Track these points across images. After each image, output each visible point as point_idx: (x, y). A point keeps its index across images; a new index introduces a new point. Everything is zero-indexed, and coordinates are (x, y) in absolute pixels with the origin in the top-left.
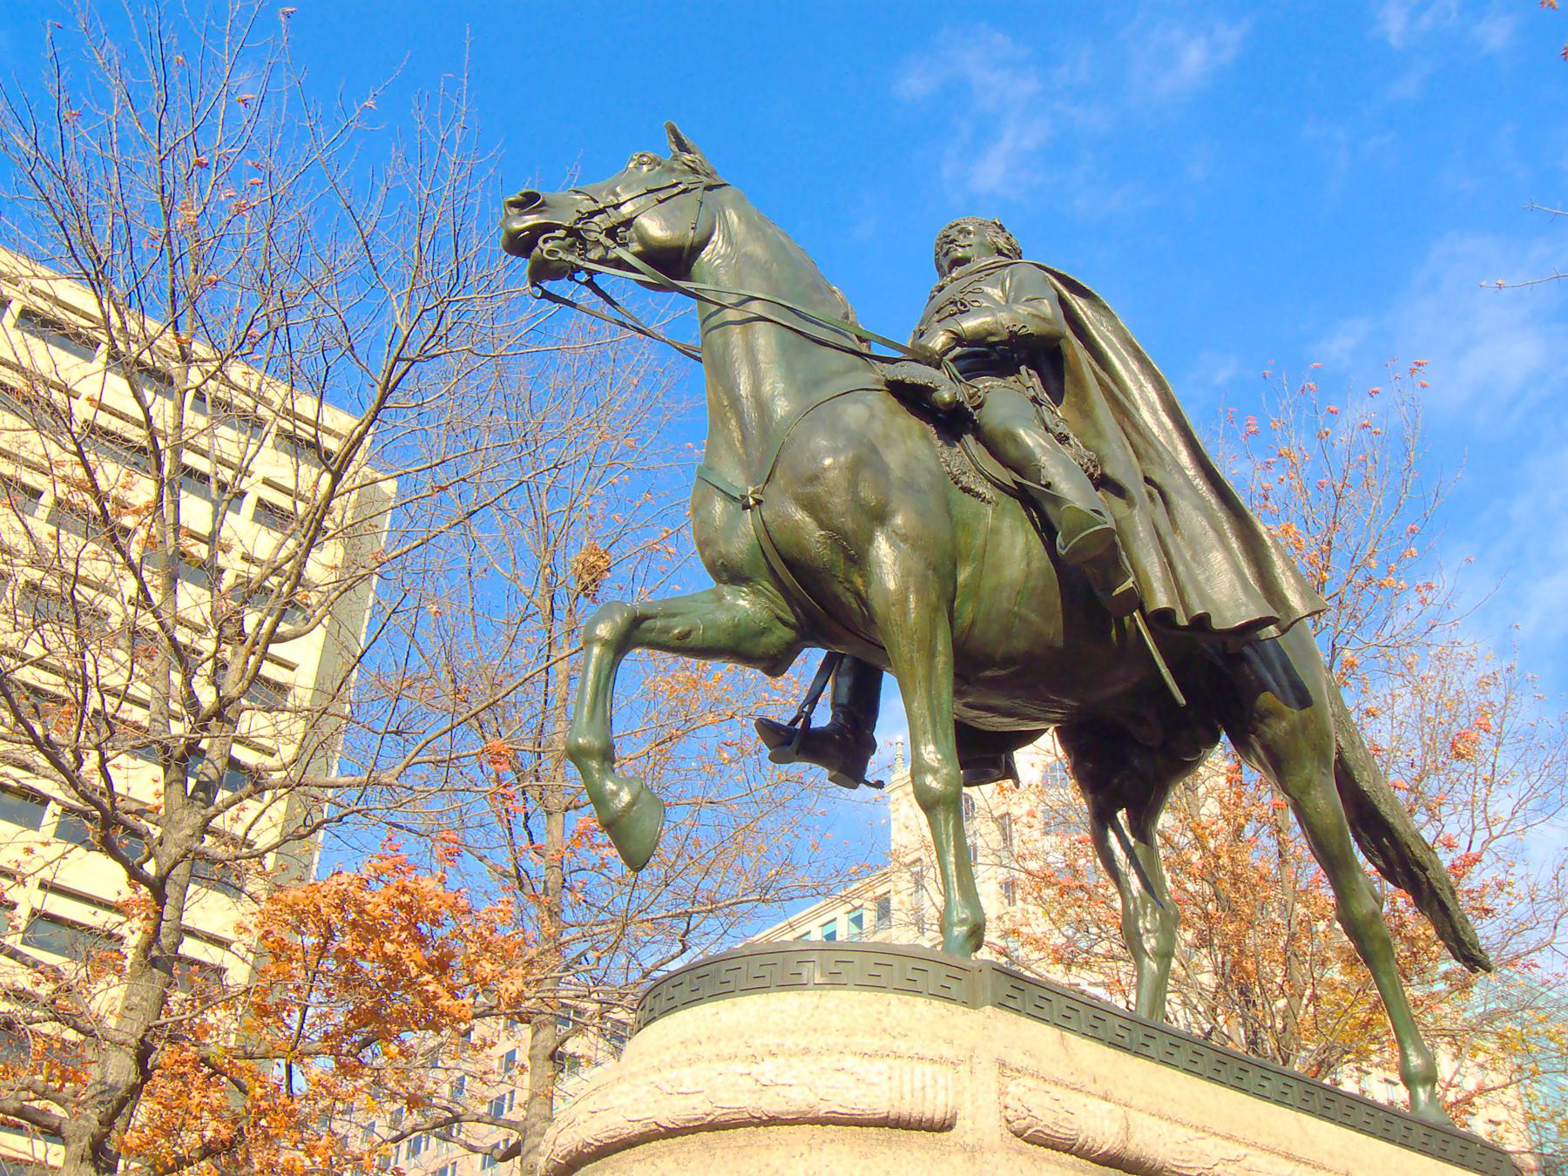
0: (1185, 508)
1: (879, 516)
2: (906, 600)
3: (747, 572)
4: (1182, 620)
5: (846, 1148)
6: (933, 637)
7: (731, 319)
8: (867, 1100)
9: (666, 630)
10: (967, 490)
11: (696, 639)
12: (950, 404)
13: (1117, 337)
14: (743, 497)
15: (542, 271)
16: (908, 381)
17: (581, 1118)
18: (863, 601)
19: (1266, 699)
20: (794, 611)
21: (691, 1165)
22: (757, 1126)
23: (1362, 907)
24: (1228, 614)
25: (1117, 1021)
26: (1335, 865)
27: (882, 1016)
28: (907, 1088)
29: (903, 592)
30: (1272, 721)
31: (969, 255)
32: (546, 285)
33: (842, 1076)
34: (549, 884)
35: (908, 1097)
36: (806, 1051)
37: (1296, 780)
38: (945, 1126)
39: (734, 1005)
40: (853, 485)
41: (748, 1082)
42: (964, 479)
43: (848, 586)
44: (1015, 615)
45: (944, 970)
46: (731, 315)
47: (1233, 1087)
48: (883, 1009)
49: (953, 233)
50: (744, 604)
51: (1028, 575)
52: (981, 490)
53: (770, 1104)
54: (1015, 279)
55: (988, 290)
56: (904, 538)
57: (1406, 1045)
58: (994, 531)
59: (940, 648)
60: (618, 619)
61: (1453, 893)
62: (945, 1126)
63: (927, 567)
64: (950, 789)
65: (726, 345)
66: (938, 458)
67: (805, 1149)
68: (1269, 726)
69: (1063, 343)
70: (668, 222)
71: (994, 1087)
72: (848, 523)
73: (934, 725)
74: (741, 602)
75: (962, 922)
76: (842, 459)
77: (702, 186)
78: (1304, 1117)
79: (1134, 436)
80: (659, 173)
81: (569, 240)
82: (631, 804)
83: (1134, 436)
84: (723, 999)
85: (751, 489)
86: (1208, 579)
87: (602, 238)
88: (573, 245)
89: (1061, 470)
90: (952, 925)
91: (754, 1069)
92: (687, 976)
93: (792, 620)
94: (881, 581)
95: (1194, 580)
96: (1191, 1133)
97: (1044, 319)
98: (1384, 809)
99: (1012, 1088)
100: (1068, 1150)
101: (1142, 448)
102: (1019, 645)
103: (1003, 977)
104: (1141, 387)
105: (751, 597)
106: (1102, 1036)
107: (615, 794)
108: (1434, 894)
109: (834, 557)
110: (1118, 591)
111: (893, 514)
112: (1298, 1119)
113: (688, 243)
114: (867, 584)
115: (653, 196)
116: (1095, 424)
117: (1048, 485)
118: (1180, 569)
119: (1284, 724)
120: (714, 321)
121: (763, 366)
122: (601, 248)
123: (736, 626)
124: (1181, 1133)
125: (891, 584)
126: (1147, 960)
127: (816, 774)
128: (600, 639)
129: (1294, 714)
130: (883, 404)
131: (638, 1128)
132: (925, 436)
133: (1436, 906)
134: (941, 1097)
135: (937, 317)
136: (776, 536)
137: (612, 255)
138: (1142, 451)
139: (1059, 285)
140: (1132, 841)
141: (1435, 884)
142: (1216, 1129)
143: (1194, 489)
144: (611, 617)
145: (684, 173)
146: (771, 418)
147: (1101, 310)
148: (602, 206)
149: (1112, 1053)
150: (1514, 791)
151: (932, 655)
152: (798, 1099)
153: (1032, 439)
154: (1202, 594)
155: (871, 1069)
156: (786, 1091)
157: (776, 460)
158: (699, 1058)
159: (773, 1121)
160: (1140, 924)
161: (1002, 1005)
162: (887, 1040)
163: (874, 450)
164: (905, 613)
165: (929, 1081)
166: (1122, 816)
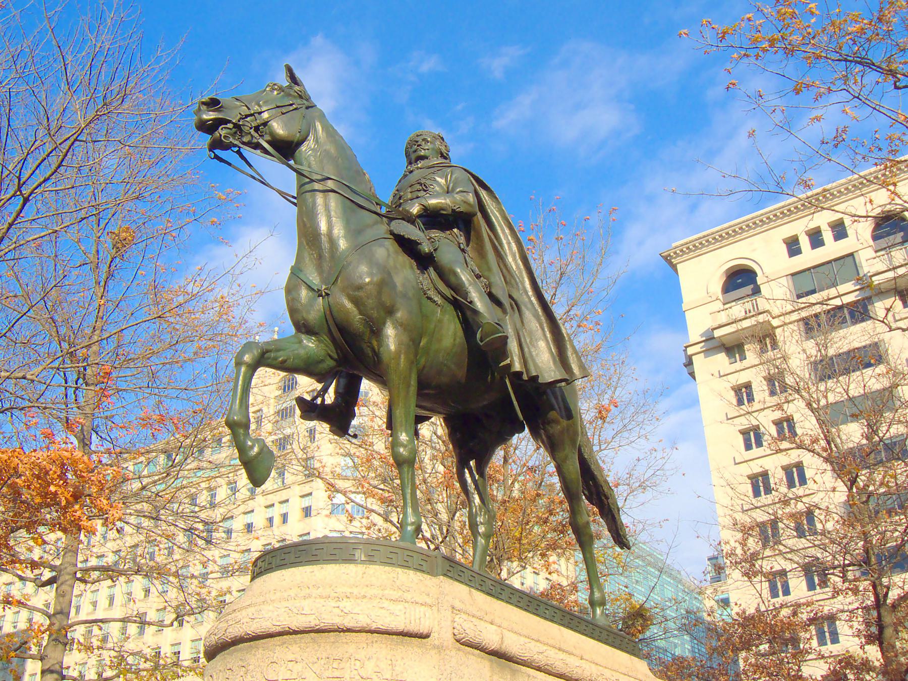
0: (528, 315)
1: (390, 311)
2: (400, 357)
3: (316, 330)
4: (525, 377)
5: (384, 646)
6: (410, 377)
7: (316, 188)
8: (394, 623)
9: (275, 359)
10: (429, 298)
11: (289, 364)
12: (426, 254)
13: (500, 214)
14: (319, 290)
15: (217, 145)
16: (406, 236)
17: (245, 620)
18: (376, 354)
19: (553, 414)
20: (337, 353)
21: (308, 650)
22: (340, 632)
23: (582, 520)
24: (546, 375)
25: (490, 582)
26: (571, 496)
27: (395, 580)
28: (413, 618)
29: (398, 353)
30: (554, 425)
31: (428, 155)
32: (218, 152)
33: (383, 611)
34: (85, 428)
35: (413, 622)
36: (365, 597)
37: (560, 455)
38: (427, 636)
39: (322, 568)
40: (380, 293)
41: (337, 611)
42: (428, 292)
43: (369, 344)
44: (445, 365)
45: (421, 557)
46: (317, 186)
47: (534, 614)
48: (395, 576)
49: (420, 139)
50: (310, 344)
51: (454, 345)
52: (436, 299)
53: (349, 623)
54: (454, 176)
55: (438, 179)
56: (401, 325)
57: (595, 590)
58: (440, 321)
59: (412, 383)
60: (256, 353)
61: (619, 511)
62: (427, 636)
63: (410, 340)
64: (412, 455)
65: (314, 203)
66: (417, 280)
67: (365, 645)
68: (552, 427)
69: (475, 219)
70: (285, 126)
71: (450, 618)
72: (375, 314)
73: (406, 421)
74: (310, 345)
75: (413, 524)
76: (375, 279)
77: (304, 107)
78: (562, 628)
79: (504, 271)
80: (283, 96)
81: (234, 130)
82: (259, 454)
83: (504, 271)
84: (316, 565)
85: (324, 287)
86: (537, 355)
87: (252, 131)
88: (236, 133)
89: (478, 295)
90: (407, 524)
91: (338, 604)
92: (293, 549)
93: (336, 356)
94: (388, 345)
95: (532, 356)
96: (527, 640)
97: (469, 204)
98: (593, 467)
99: (457, 619)
100: (476, 648)
101: (508, 277)
102: (444, 380)
103: (446, 561)
104: (509, 243)
105: (317, 343)
106: (484, 589)
107: (252, 447)
108: (610, 510)
109: (365, 330)
110: (502, 364)
111: (398, 310)
112: (559, 629)
113: (296, 140)
114: (380, 346)
115: (279, 110)
116: (487, 263)
117: (471, 302)
118: (526, 350)
119: (559, 427)
120: (308, 187)
121: (334, 219)
122: (249, 136)
123: (309, 358)
124: (523, 639)
125: (392, 347)
126: (479, 538)
127: (323, 428)
128: (246, 363)
129: (564, 422)
130: (391, 245)
131: (279, 629)
132: (412, 268)
133: (610, 517)
134: (427, 623)
135: (409, 190)
136: (335, 314)
137: (255, 141)
138: (508, 280)
139: (474, 182)
140: (477, 477)
141: (611, 506)
142: (533, 637)
143: (531, 302)
144: (252, 352)
145: (295, 97)
146: (337, 249)
147: (494, 200)
148: (252, 112)
149: (489, 598)
150: (615, 426)
151: (408, 386)
152: (362, 621)
153: (465, 277)
154: (535, 365)
155: (398, 608)
156: (356, 616)
157: (340, 272)
158: (310, 596)
159: (349, 630)
160: (478, 519)
161: (445, 575)
162: (401, 593)
163: (389, 274)
164: (398, 364)
165: (422, 615)
166: (472, 463)
